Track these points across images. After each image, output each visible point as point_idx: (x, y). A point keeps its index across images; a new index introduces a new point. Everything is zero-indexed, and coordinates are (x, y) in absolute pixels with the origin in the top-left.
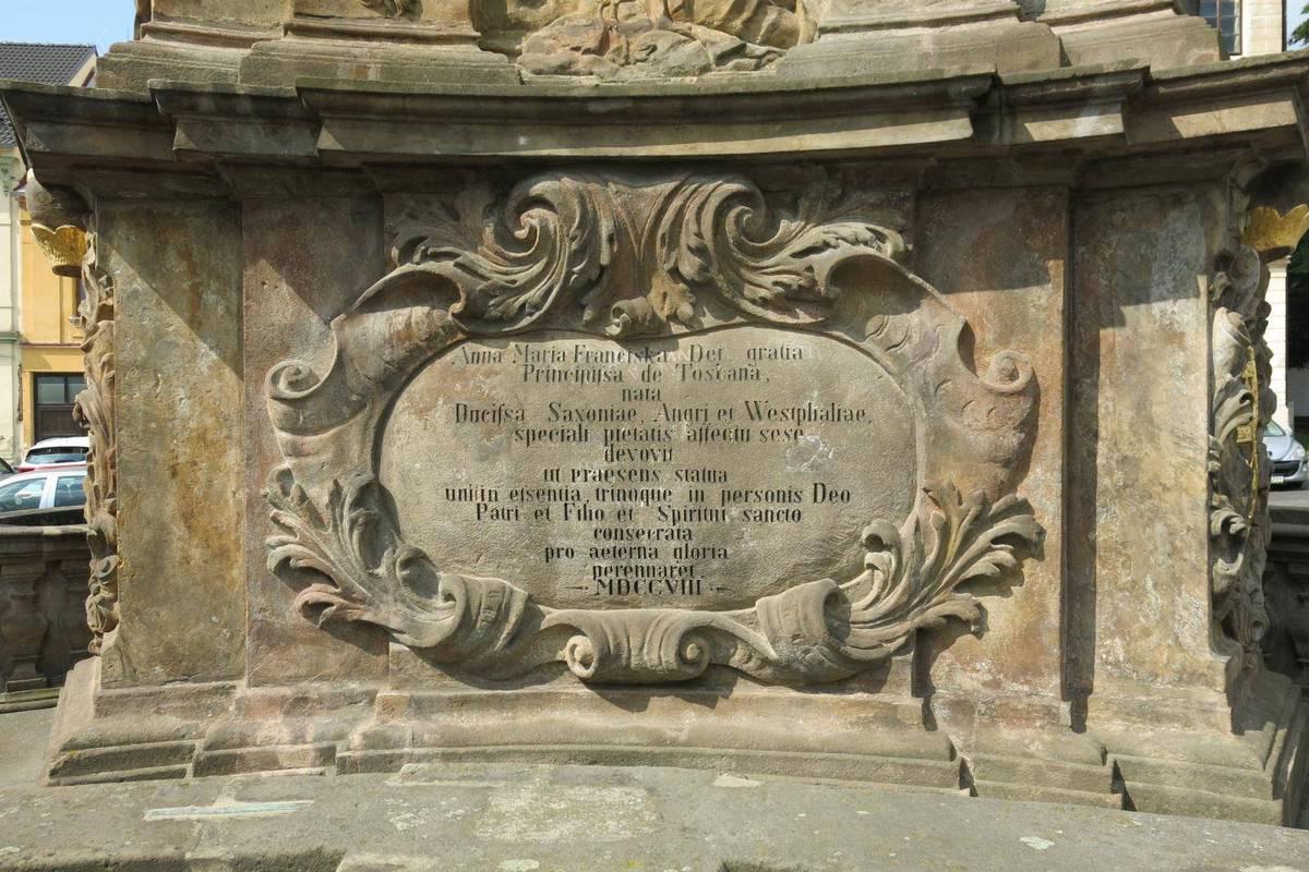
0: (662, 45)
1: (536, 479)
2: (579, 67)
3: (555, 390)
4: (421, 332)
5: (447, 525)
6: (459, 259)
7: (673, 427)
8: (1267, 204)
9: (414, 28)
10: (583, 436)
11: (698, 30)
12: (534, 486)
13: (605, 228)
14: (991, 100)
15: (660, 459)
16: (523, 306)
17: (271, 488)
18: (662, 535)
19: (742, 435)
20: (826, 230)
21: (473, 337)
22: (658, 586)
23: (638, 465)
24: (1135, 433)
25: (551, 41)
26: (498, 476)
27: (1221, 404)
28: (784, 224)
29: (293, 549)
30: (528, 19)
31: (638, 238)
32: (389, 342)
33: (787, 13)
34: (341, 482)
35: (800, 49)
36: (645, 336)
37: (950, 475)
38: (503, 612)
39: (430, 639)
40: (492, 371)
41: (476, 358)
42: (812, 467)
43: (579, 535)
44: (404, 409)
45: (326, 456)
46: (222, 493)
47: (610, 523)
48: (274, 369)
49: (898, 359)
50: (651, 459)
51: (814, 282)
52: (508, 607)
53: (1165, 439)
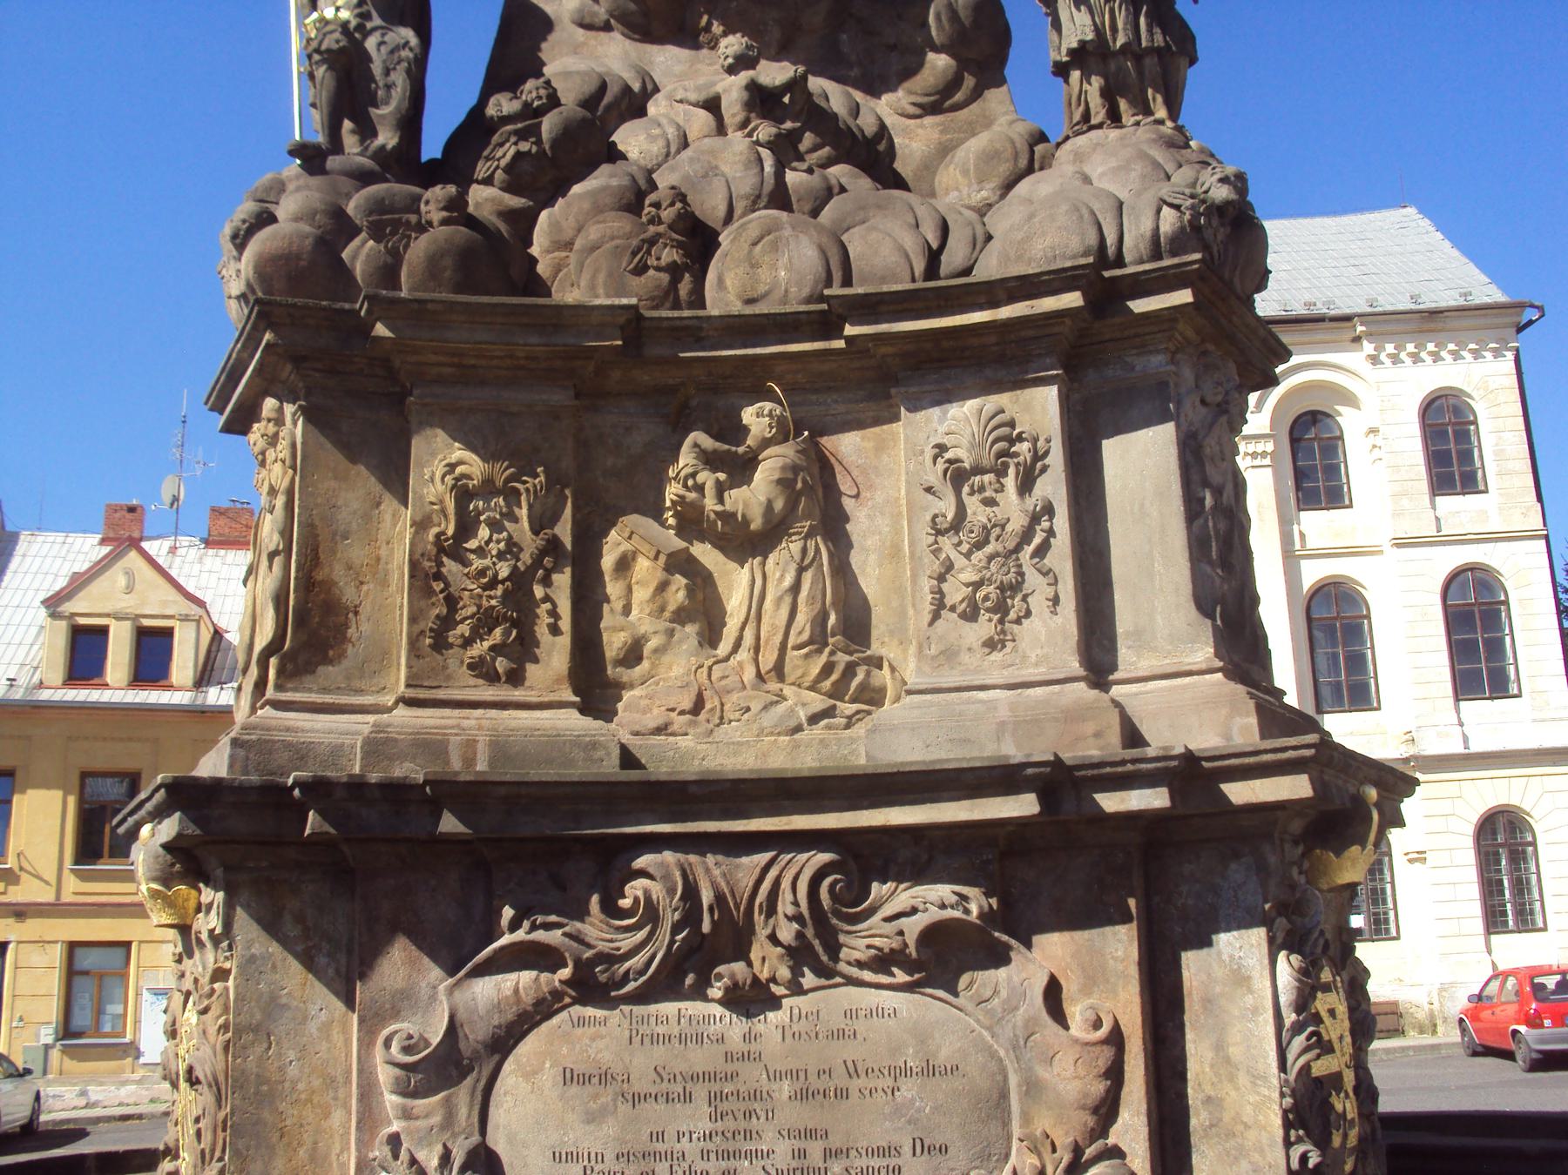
0: (756, 707)
1: (642, 1142)
2: (675, 727)
3: (659, 1053)
4: (528, 999)
6: (567, 929)
8: (1323, 848)
9: (518, 694)
10: (687, 1097)
11: (788, 691)
12: (639, 1148)
13: (707, 897)
14: (1060, 783)
15: (763, 1118)
16: (627, 972)
17: (380, 1151)
19: (842, 1094)
21: (582, 1001)
23: (742, 1125)
24: (1217, 1074)
25: (647, 702)
26: (601, 1139)
27: (1289, 1043)
28: (875, 886)
30: (625, 679)
31: (737, 906)
32: (498, 1007)
33: (875, 671)
34: (449, 1145)
35: (888, 711)
36: (751, 999)
37: (1044, 1122)
41: (582, 1022)
42: (909, 1122)
44: (512, 1072)
45: (436, 1119)
46: (327, 1157)
48: (386, 1032)
49: (989, 1013)
50: (754, 1118)
51: (906, 945)
53: (1243, 1079)
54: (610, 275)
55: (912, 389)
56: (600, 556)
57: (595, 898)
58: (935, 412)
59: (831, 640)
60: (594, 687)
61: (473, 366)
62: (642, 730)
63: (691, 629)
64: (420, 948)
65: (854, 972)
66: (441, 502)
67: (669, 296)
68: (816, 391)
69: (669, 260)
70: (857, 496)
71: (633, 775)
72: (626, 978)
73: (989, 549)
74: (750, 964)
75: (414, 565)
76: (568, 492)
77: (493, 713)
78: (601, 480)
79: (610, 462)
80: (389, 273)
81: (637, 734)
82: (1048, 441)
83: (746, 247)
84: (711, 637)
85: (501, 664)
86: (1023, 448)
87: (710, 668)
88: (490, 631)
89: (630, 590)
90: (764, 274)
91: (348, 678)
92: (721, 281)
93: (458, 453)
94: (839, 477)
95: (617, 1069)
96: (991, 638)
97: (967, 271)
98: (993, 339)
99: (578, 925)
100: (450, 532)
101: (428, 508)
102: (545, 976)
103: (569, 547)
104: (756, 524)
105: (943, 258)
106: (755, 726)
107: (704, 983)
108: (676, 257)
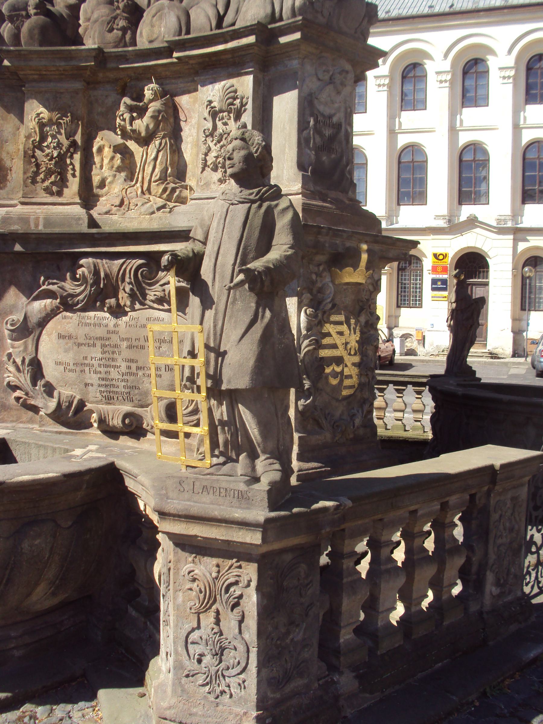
0: (140, 204)
3: (87, 329)
4: (49, 309)
5: (56, 373)
7: (122, 343)
10: (94, 345)
12: (80, 362)
13: (102, 275)
16: (78, 301)
18: (119, 380)
20: (334, 350)
21: (66, 310)
22: (120, 398)
23: (111, 356)
29: (11, 379)
30: (100, 193)
32: (40, 311)
34: (25, 357)
38: (71, 404)
39: (49, 411)
40: (67, 322)
41: (65, 317)
43: (94, 379)
45: (21, 349)
47: (103, 375)
51: (165, 295)
52: (73, 402)
54: (100, 33)
55: (202, 78)
56: (93, 147)
57: (68, 274)
58: (210, 87)
59: (168, 179)
60: (88, 198)
61: (45, 75)
62: (101, 213)
63: (123, 174)
64: (19, 290)
65: (151, 304)
66: (34, 128)
67: (121, 42)
68: (175, 78)
69: (122, 25)
70: (186, 121)
71: (94, 231)
72: (78, 303)
73: (222, 143)
74: (118, 300)
75: (25, 152)
76: (80, 123)
77: (51, 207)
78: (96, 117)
79: (100, 110)
80: (16, 38)
81: (99, 214)
82: (248, 98)
83: (150, 18)
84: (131, 177)
85: (55, 189)
86: (238, 102)
87: (127, 189)
88: (51, 176)
89: (102, 160)
90: (156, 30)
91: (8, 194)
92: (141, 33)
93: (42, 109)
94: (180, 113)
95: (74, 334)
96: (220, 179)
97: (233, 24)
98: (229, 56)
99: (63, 283)
100: (38, 140)
101: (30, 131)
102: (54, 301)
103: (80, 144)
104: (143, 134)
105: (225, 19)
106: (139, 211)
107: (103, 304)
108: (125, 24)
